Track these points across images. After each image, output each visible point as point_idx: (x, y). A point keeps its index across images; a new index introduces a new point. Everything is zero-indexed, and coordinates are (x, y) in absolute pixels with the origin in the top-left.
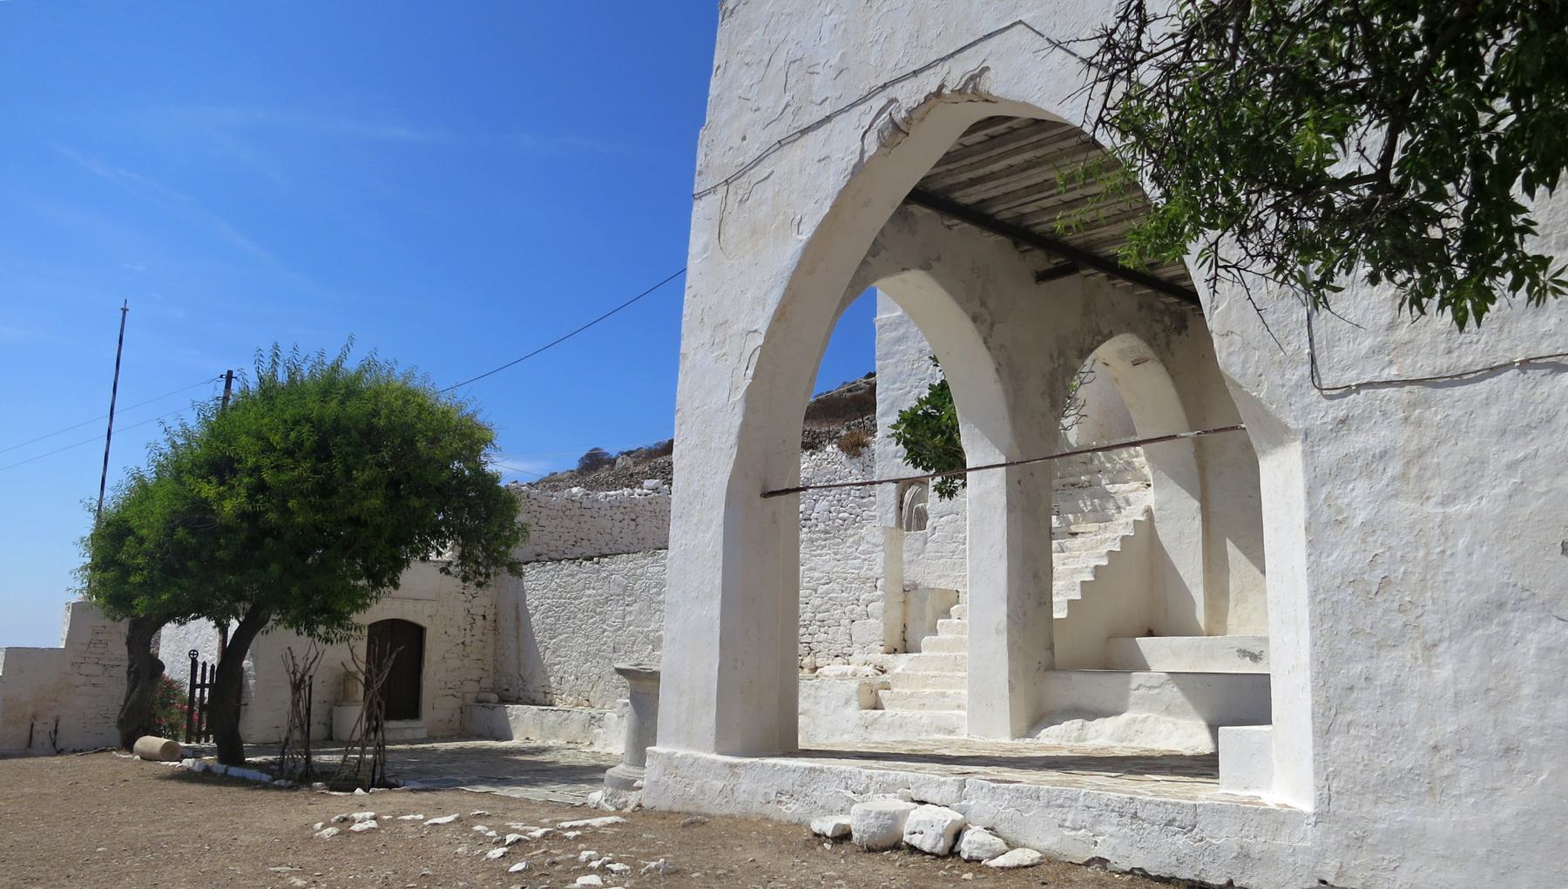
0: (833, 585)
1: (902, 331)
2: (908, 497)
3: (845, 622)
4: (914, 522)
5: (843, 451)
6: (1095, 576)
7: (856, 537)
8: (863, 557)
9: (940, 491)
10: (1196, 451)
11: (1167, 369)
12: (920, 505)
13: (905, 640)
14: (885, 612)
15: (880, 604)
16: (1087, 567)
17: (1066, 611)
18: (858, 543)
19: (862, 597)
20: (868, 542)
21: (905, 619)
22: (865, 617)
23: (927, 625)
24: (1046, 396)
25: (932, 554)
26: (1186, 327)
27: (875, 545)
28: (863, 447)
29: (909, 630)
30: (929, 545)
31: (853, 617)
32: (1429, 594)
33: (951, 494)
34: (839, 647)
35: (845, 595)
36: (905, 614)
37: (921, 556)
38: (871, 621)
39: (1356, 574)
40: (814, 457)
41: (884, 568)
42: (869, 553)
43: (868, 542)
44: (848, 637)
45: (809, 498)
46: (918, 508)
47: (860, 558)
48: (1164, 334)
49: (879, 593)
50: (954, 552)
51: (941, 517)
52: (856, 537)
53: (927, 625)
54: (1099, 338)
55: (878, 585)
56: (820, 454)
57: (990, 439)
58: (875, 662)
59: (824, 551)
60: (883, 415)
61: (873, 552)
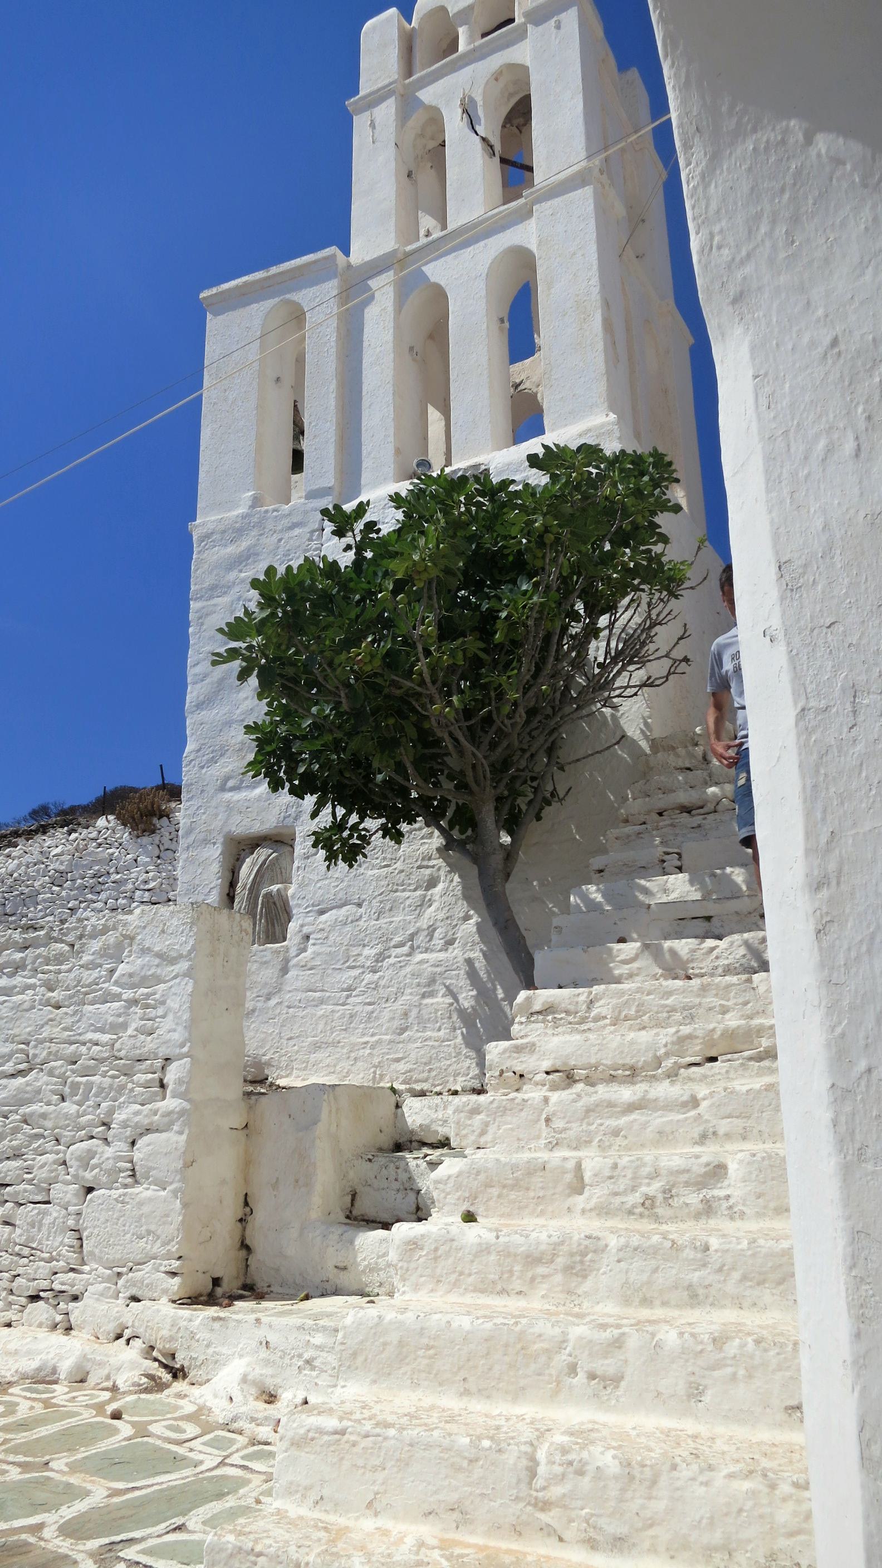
0: (37, 1079)
1: (244, 544)
2: (247, 871)
3: (65, 1192)
5: (124, 824)
7: (111, 937)
8: (129, 994)
9: (328, 846)
12: (275, 888)
13: (245, 1247)
14: (189, 1164)
15: (174, 1139)
18: (115, 954)
19: (119, 1116)
20: (145, 951)
21: (246, 1181)
22: (124, 1178)
23: (316, 1200)
25: (300, 995)
27: (166, 958)
28: (160, 817)
29: (261, 1217)
30: (292, 974)
31: (89, 1176)
33: (352, 854)
34: (43, 1269)
35: (69, 1107)
36: (247, 1164)
37: (273, 1002)
38: (143, 1192)
40: (74, 836)
41: (192, 1025)
42: (145, 981)
43: (145, 951)
44: (69, 1239)
45: (63, 906)
46: (269, 895)
47: (117, 998)
49: (171, 1103)
50: (350, 989)
51: (322, 912)
52: (111, 937)
53: (316, 1200)
55: (170, 1078)
56: (85, 831)
58: (150, 1336)
59: (18, 980)
60: (199, 706)
61: (159, 980)
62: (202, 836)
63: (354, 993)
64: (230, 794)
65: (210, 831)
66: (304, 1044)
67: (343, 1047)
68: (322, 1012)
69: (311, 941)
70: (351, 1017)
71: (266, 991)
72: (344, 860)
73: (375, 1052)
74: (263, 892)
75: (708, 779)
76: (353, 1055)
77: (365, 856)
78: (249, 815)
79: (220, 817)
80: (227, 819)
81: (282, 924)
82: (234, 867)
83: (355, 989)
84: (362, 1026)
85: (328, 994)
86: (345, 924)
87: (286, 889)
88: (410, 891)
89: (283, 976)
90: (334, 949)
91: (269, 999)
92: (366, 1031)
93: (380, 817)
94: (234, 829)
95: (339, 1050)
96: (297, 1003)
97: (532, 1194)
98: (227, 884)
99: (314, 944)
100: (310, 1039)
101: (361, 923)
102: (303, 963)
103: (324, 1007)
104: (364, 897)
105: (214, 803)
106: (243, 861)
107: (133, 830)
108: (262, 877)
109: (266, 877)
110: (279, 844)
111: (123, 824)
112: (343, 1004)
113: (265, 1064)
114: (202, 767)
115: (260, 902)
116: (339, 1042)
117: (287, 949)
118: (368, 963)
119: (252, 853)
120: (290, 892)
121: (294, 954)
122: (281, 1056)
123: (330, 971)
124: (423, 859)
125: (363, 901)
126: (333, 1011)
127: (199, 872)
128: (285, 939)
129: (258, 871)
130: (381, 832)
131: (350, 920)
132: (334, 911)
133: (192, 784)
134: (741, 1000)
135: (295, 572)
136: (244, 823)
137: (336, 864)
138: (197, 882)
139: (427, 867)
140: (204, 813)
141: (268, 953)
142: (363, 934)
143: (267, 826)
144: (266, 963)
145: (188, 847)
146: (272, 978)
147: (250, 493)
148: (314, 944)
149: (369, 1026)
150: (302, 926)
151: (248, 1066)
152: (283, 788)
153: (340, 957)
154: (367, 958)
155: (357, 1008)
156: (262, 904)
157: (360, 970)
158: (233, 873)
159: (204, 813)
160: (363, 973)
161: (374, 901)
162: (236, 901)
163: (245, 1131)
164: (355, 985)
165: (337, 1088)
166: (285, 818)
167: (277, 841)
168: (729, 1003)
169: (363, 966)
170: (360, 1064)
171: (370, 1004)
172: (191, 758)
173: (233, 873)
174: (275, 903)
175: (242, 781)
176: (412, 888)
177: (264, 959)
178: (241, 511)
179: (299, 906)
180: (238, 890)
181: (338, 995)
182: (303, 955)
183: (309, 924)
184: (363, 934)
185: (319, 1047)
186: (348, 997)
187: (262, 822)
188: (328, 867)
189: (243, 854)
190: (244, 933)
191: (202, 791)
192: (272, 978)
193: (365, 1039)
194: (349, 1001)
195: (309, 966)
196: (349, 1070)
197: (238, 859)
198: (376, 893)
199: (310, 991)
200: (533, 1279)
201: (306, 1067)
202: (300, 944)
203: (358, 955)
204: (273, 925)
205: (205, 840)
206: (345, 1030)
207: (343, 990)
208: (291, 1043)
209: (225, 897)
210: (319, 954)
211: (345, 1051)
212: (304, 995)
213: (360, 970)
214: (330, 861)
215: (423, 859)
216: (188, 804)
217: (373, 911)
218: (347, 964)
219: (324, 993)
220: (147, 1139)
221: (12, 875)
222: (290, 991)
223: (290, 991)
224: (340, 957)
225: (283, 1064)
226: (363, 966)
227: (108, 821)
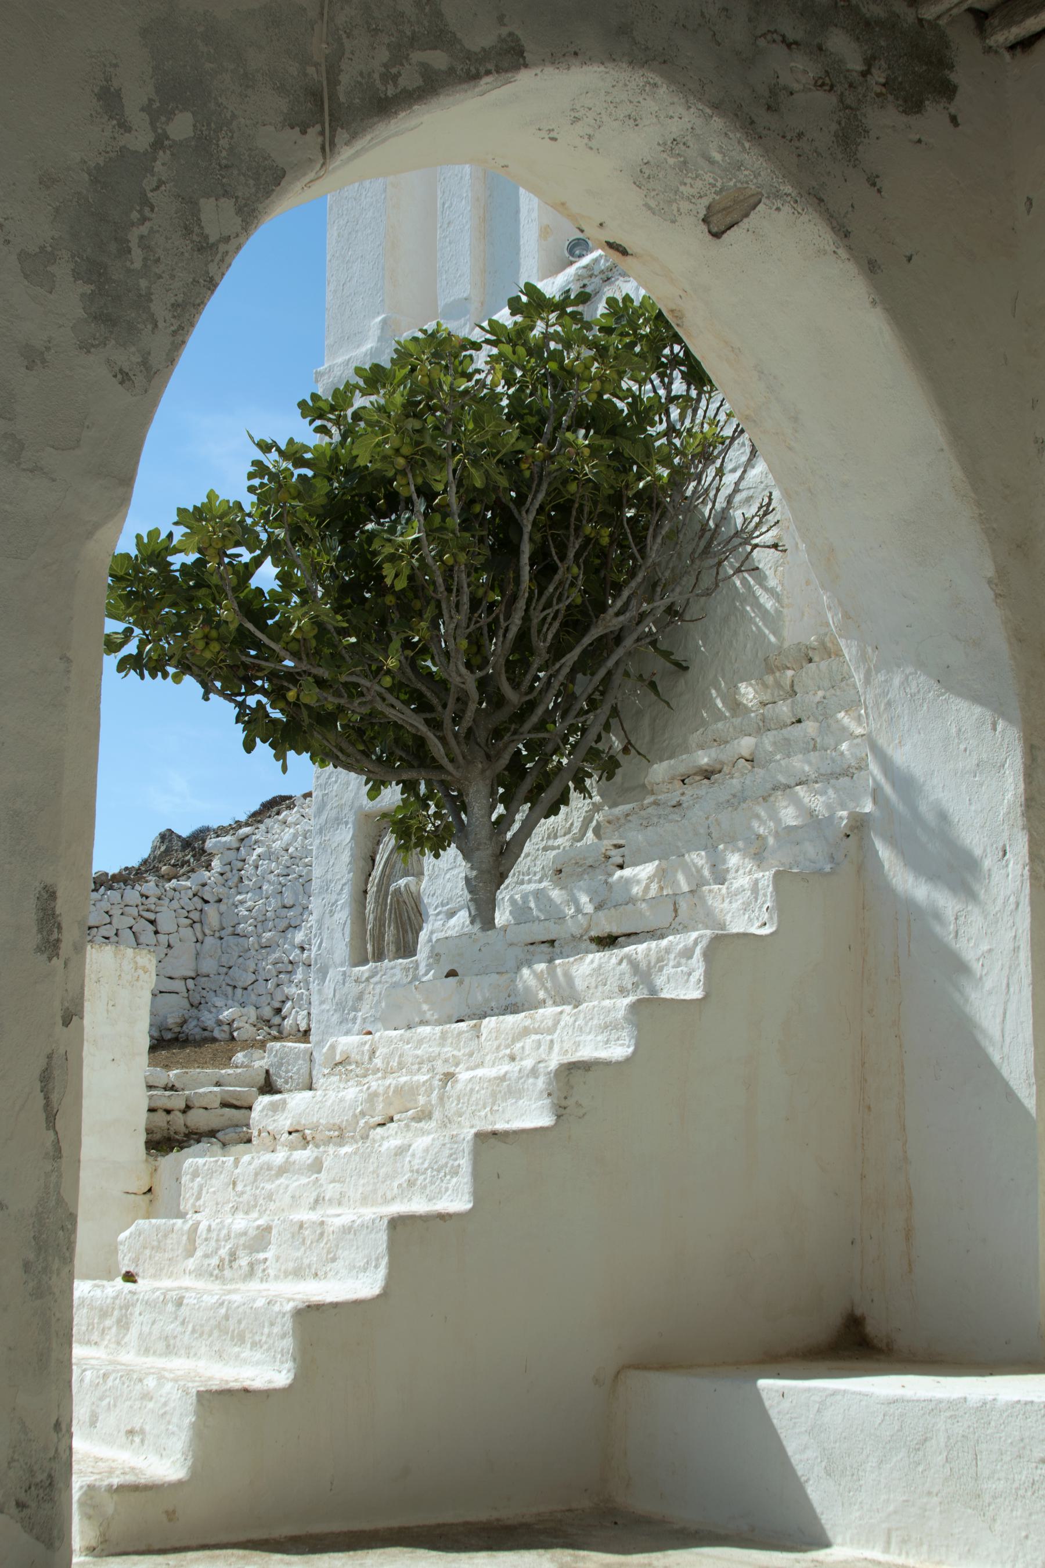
4: (390, 934)
6: (560, 1111)
10: (1002, 572)
11: (843, 233)
12: (402, 882)
16: (534, 1072)
17: (382, 1272)
24: (62, 270)
26: (948, 90)
32: (85, 1311)
39: (284, 1018)
46: (398, 891)
48: (826, 100)
54: (439, 60)
57: (1024, 735)
75: (761, 724)
87: (418, 884)
88: (535, 882)
97: (166, 1255)
108: (393, 867)
124: (549, 838)
129: (388, 859)
134: (467, 1050)
135: (146, 540)
138: (329, 876)
139: (553, 848)
141: (397, 971)
147: (380, 318)
150: (432, 933)
159: (336, 782)
163: (148, 1196)
168: (460, 1054)
176: (537, 878)
178: (369, 346)
190: (140, 972)
200: (103, 1330)
204: (405, 932)
215: (549, 838)
221: (287, 850)
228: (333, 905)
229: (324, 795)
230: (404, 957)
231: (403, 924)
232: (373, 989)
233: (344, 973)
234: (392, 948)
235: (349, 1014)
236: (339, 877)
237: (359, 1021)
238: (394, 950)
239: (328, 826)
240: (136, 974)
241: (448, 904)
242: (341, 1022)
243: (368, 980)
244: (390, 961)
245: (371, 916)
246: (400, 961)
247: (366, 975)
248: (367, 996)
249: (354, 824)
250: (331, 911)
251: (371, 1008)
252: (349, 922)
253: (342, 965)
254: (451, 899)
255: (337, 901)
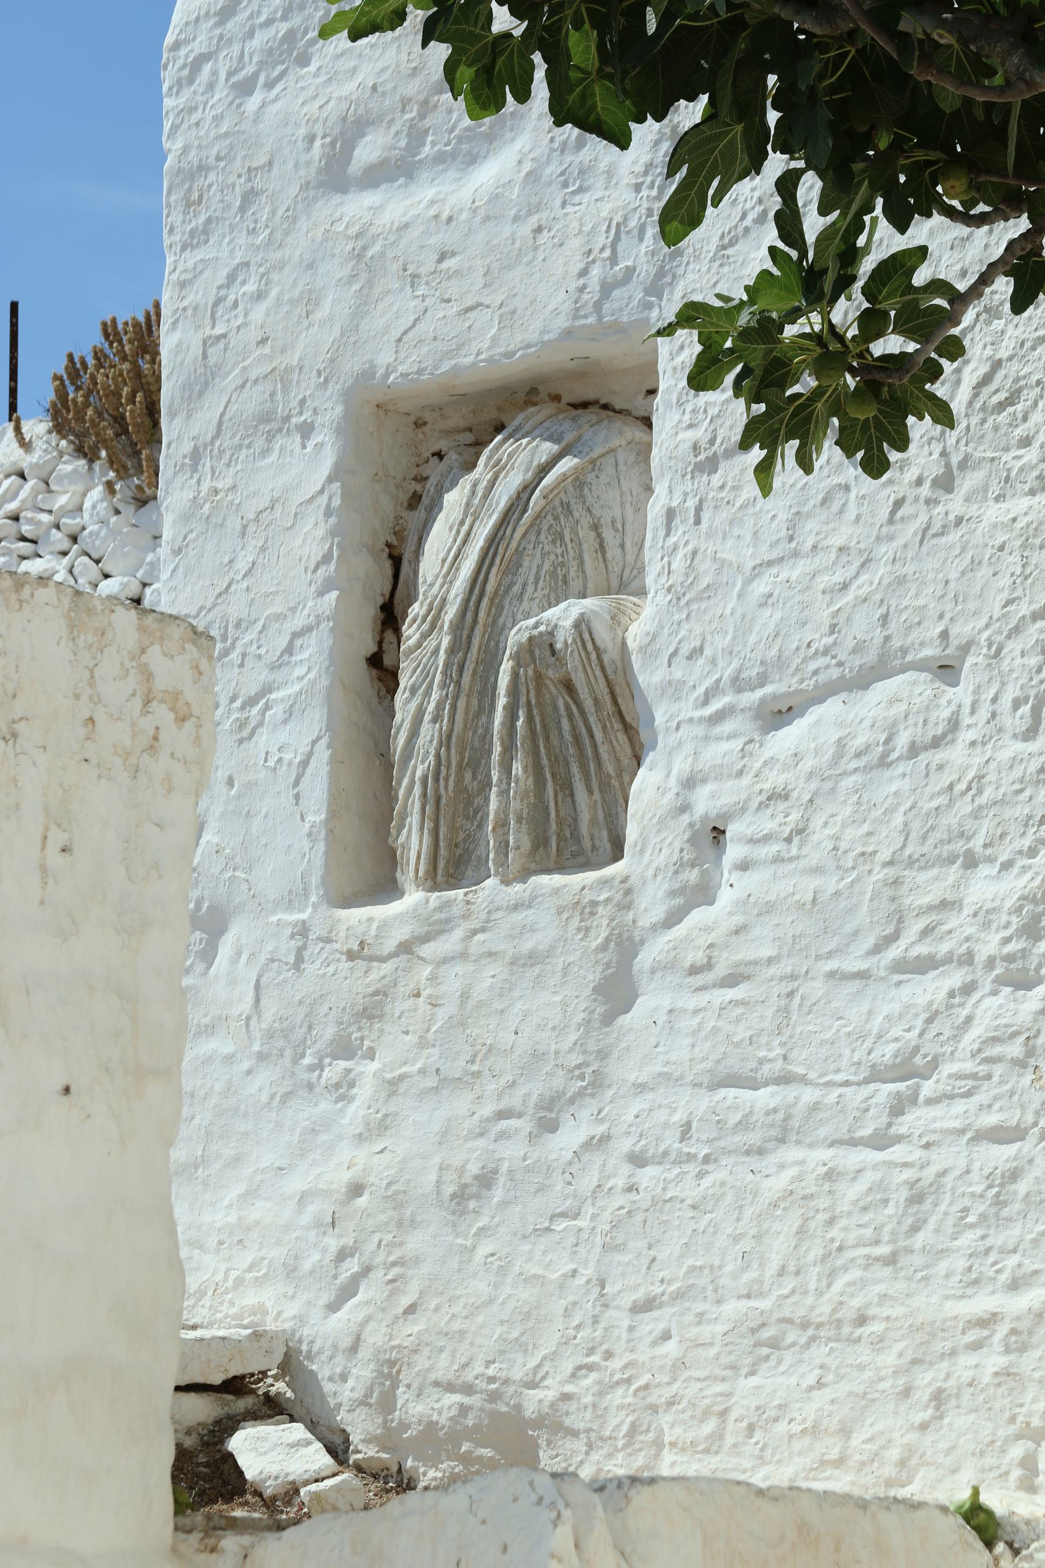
5: (85, 451)
7: (683, 602)
62: (252, 400)
63: (928, 1088)
64: (370, 198)
65: (284, 378)
66: (707, 1331)
67: (879, 1343)
68: (780, 1182)
69: (733, 852)
70: (916, 1199)
71: (534, 1089)
72: (847, 444)
73: (1027, 1362)
74: (516, 636)
76: (926, 1379)
77: (943, 415)
78: (453, 289)
79: (323, 312)
80: (359, 313)
81: (605, 787)
82: (399, 533)
83: (934, 1064)
84: (968, 1239)
85: (808, 1095)
86: (884, 762)
87: (617, 619)
89: (608, 1019)
90: (831, 884)
91: (552, 1127)
92: (984, 1267)
93: (1001, 213)
94: (384, 358)
95: (863, 1354)
96: (671, 1141)
98: (369, 614)
99: (744, 866)
100: (733, 1308)
101: (956, 754)
102: (695, 956)
103: (792, 1153)
104: (961, 631)
105: (299, 245)
106: (435, 507)
107: (122, 472)
108: (514, 566)
109: (529, 566)
110: (587, 416)
111: (80, 451)
112: (881, 1141)
113: (539, 1423)
114: (246, 88)
115: (504, 680)
116: (862, 1320)
117: (628, 893)
118: (990, 945)
119: (471, 466)
120: (636, 633)
121: (658, 913)
122: (604, 1389)
123: (816, 988)
125: (965, 649)
126: (831, 1175)
127: (242, 565)
128: (617, 854)
129: (493, 541)
130: (1003, 287)
131: (902, 741)
132: (832, 707)
133: (203, 168)
136: (426, 328)
137: (805, 463)
140: (259, 296)
142: (965, 807)
143: (532, 334)
144: (533, 958)
145: (196, 456)
146: (560, 1030)
148: (744, 866)
149: (998, 1239)
150: (690, 783)
151: (468, 1434)
152: (523, 95)
153: (862, 916)
154: (985, 917)
155: (940, 1159)
156: (514, 691)
157: (956, 978)
158: (397, 561)
159: (259, 296)
160: (968, 989)
161: (1014, 647)
162: (405, 680)
164: (930, 1048)
165: (641, 1497)
166: (607, 288)
167: (585, 405)
169: (968, 959)
170: (958, 1420)
171: (1000, 1135)
172: (198, 47)
173: (397, 561)
174: (569, 687)
175: (417, 136)
177: (527, 945)
179: (674, 689)
180: (410, 632)
181: (855, 1097)
182: (698, 916)
183: (720, 773)
184: (965, 807)
185: (775, 1344)
186: (898, 1108)
187: (508, 318)
188: (764, 471)
189: (435, 470)
190: (162, 713)
191: (249, 197)
192: (560, 1030)
193: (982, 1304)
194: (904, 1124)
195: (720, 970)
196: (910, 1450)
197: (414, 501)
198: (1024, 609)
199: (733, 1081)
201: (718, 1436)
202: (680, 866)
203: (944, 905)
204: (566, 787)
205: (266, 417)
206: (891, 1260)
207: (876, 1075)
208: (651, 1324)
209: (362, 673)
210: (768, 909)
211: (889, 1359)
212: (704, 1102)
213: (956, 978)
214: (772, 444)
216: (192, 258)
217: (1011, 692)
218: (894, 952)
219: (790, 1092)
220: (319, 487)
222: (641, 1088)
223: (641, 1088)
224: (862, 916)
225: (618, 1422)
226: (968, 959)
227: (25, 445)
228: (251, 702)
229: (207, 343)
230: (560, 867)
231: (558, 760)
232: (433, 978)
233: (302, 930)
234: (518, 837)
235: (320, 1067)
236: (276, 609)
237: (364, 1092)
238: (526, 845)
239: (227, 441)
240: (147, 724)
241: (762, 680)
242: (287, 1097)
243: (406, 948)
244: (506, 882)
245: (428, 732)
246: (545, 880)
247: (402, 933)
248: (401, 1006)
249: (339, 431)
250: (242, 724)
251: (423, 1044)
252: (322, 755)
253: (291, 901)
254: (780, 661)
255: (267, 689)
